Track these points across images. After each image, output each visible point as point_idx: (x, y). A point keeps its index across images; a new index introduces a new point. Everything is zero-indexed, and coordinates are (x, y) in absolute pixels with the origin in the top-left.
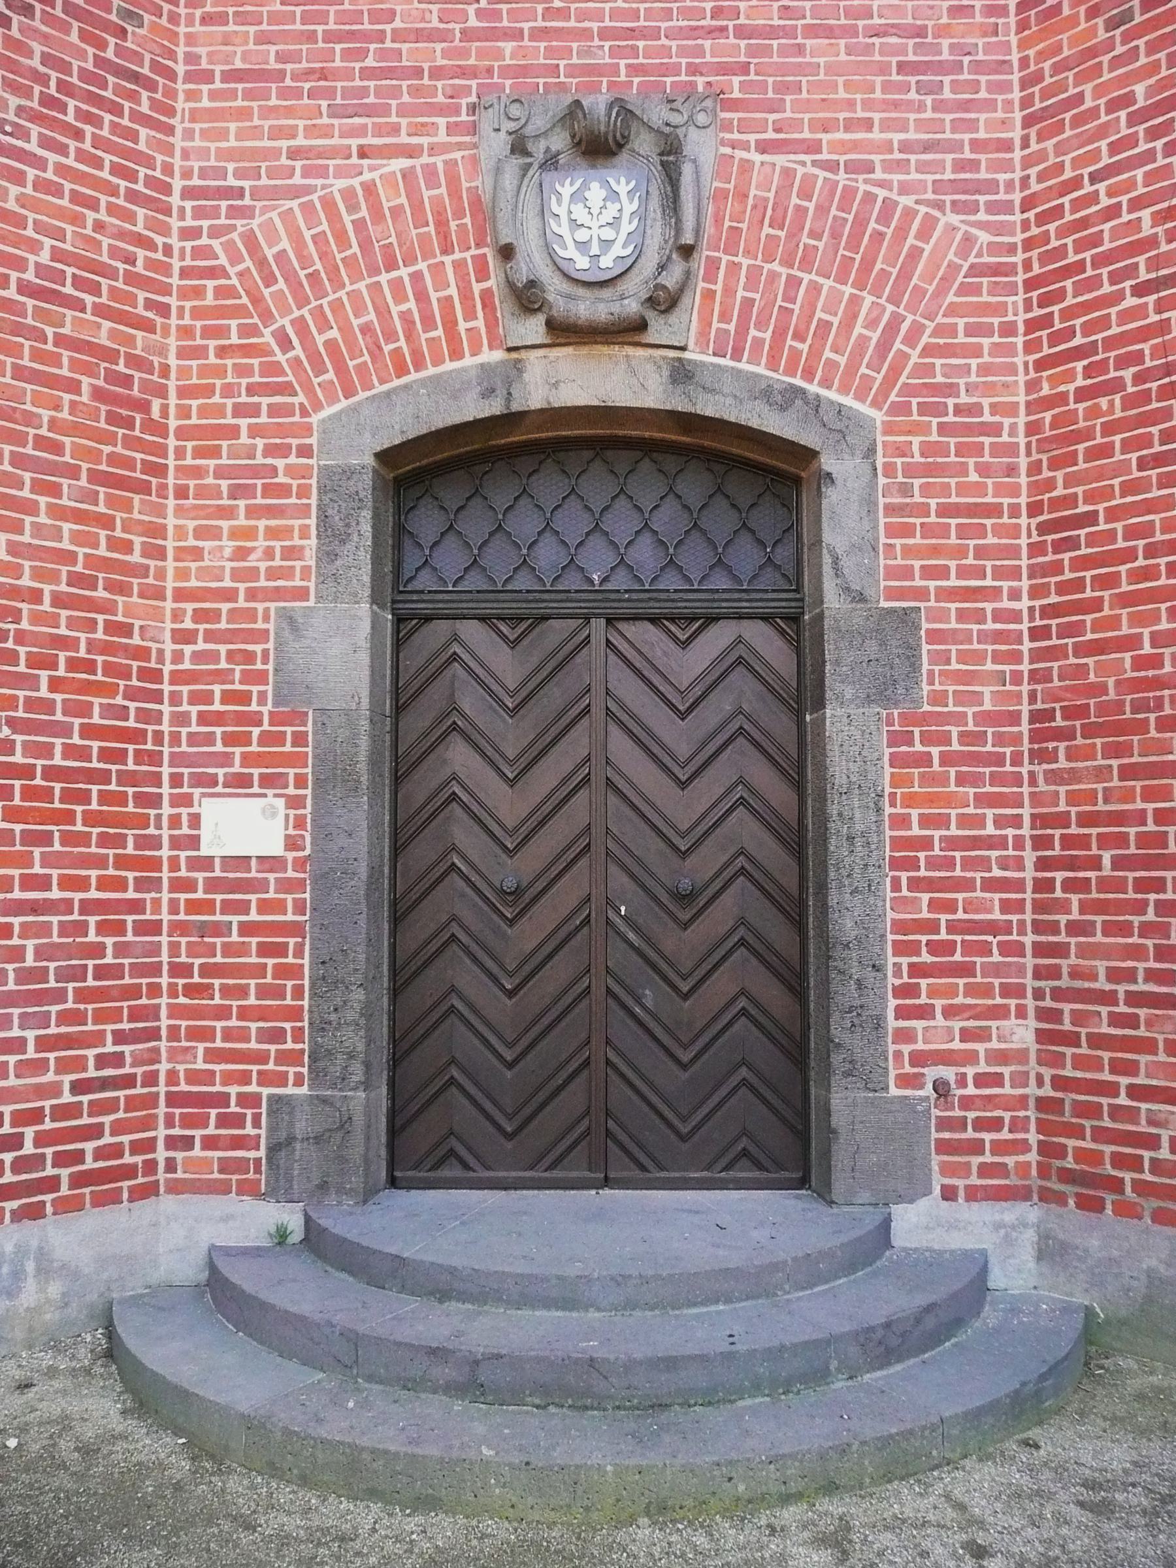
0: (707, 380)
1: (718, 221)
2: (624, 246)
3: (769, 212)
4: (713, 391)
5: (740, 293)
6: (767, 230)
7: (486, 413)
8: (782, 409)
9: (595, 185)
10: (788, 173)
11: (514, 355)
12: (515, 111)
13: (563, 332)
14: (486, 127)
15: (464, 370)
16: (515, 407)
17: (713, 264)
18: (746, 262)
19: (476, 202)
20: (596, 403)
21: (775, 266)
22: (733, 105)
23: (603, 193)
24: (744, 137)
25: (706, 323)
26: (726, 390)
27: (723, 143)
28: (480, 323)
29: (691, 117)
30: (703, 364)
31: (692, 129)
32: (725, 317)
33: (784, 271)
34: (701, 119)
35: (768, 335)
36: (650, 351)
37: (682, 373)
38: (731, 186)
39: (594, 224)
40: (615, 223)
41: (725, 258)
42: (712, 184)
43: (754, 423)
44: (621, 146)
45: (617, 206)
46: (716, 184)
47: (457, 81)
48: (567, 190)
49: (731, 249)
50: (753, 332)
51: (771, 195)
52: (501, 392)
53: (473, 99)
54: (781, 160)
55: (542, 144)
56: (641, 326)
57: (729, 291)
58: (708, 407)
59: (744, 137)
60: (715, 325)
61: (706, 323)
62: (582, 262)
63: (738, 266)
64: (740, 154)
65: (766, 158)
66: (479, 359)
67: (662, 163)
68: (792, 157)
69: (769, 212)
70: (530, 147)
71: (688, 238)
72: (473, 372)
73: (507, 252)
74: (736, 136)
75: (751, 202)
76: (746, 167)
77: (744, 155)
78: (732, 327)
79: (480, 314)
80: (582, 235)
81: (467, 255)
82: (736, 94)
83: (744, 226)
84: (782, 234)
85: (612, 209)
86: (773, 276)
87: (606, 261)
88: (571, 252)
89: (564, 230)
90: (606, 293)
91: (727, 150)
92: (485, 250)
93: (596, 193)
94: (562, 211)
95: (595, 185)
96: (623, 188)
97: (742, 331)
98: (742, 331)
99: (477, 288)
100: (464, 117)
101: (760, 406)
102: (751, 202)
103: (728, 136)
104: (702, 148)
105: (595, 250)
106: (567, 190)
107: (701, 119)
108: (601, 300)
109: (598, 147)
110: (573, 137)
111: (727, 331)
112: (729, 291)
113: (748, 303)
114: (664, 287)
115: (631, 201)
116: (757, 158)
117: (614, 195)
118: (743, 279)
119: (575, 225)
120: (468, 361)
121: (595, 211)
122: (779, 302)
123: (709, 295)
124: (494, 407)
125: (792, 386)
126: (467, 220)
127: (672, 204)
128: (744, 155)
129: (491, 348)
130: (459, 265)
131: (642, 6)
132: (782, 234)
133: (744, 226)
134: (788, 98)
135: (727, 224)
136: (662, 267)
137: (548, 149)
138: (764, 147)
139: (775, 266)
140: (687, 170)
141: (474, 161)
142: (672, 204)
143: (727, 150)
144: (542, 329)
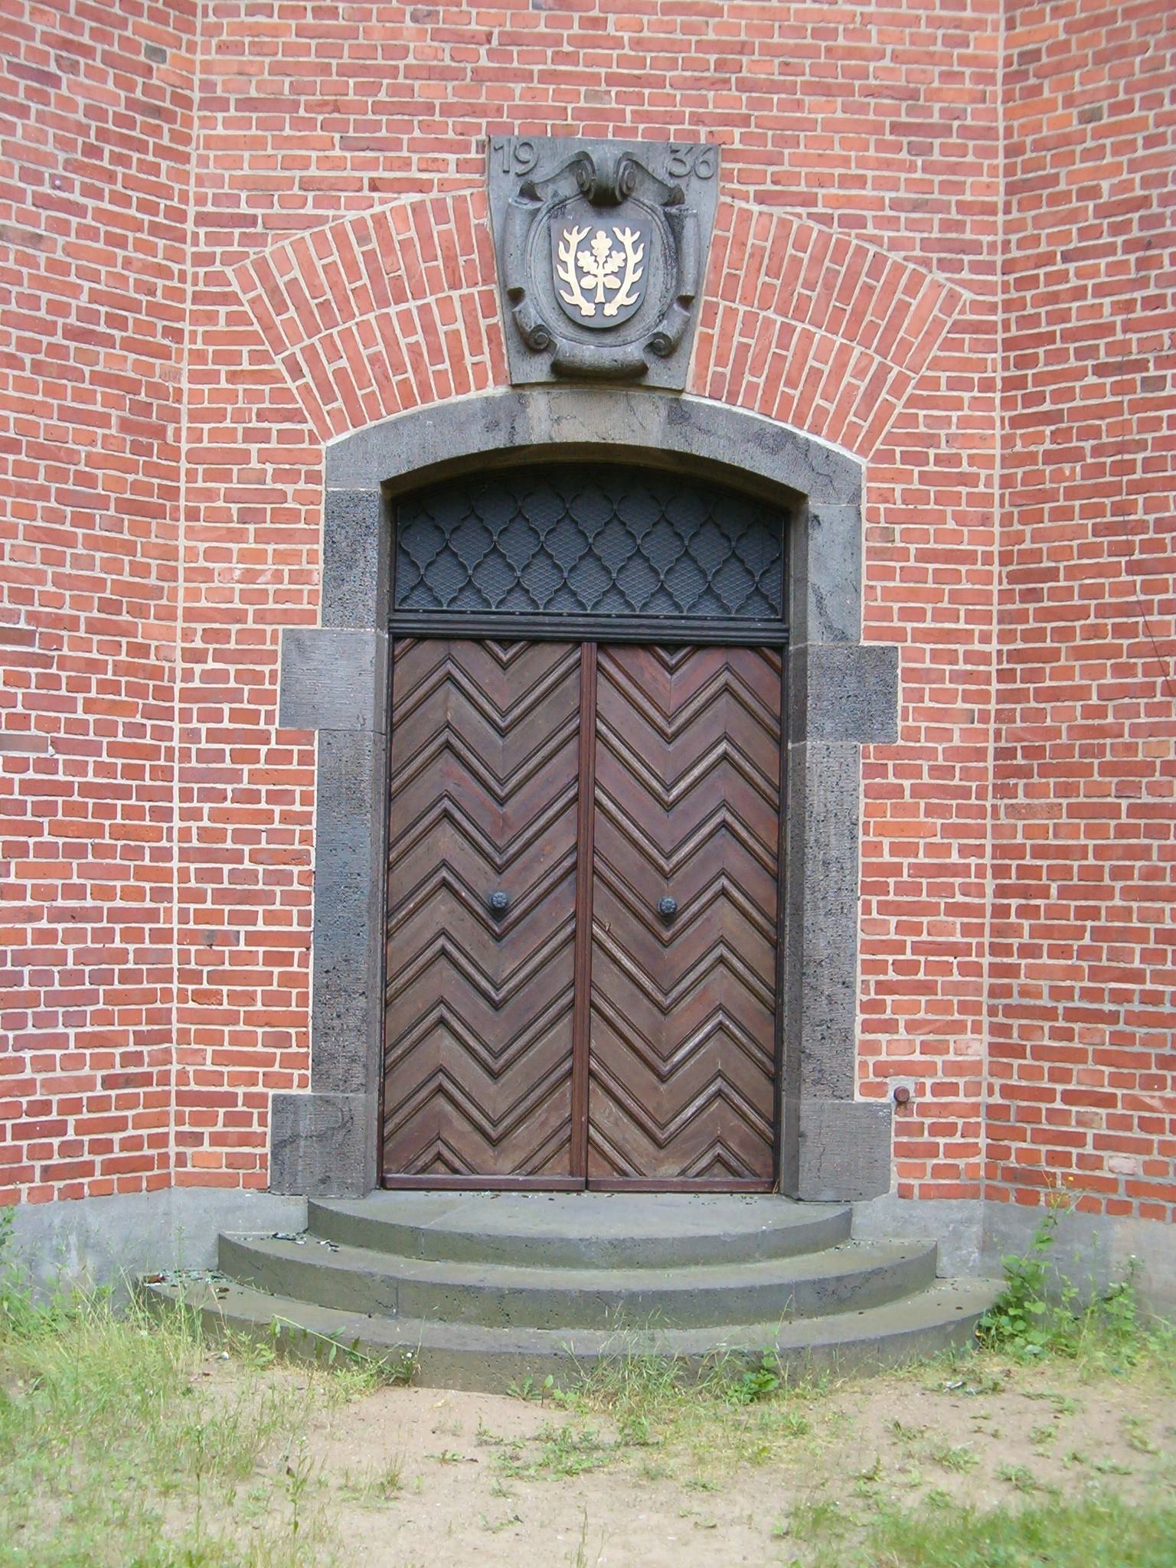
1: (717, 267)
2: (628, 295)
3: (766, 261)
6: (764, 278)
7: (491, 447)
8: (774, 451)
9: (601, 234)
12: (524, 154)
14: (496, 169)
15: (469, 402)
16: (519, 441)
17: (711, 308)
18: (742, 309)
20: (595, 440)
21: (770, 314)
23: (609, 243)
25: (702, 365)
28: (486, 357)
29: (693, 168)
32: (721, 361)
33: (780, 319)
35: (762, 381)
37: (679, 413)
38: (730, 235)
39: (600, 272)
40: (620, 274)
41: (723, 304)
43: (747, 466)
44: (625, 196)
46: (716, 232)
48: (574, 238)
50: (748, 377)
52: (505, 425)
53: (483, 137)
54: (778, 211)
55: (551, 189)
56: (641, 370)
57: (726, 336)
58: (702, 447)
59: (744, 188)
60: (712, 368)
61: (702, 365)
62: (588, 309)
65: (764, 208)
67: (668, 216)
68: (789, 209)
69: (766, 261)
71: (688, 290)
73: (515, 296)
74: (736, 186)
75: (748, 250)
76: (745, 216)
77: (744, 205)
78: (728, 371)
79: (486, 349)
80: (588, 282)
81: (474, 290)
82: (737, 145)
83: (742, 273)
85: (617, 259)
86: (768, 323)
88: (577, 299)
89: (570, 277)
90: (609, 339)
91: (728, 200)
93: (602, 242)
94: (568, 258)
95: (601, 234)
96: (628, 239)
98: (738, 374)
99: (483, 323)
100: (473, 155)
102: (748, 250)
103: (729, 186)
104: (701, 201)
105: (600, 297)
106: (574, 238)
107: (703, 171)
109: (605, 200)
110: (581, 185)
114: (665, 337)
116: (756, 208)
117: (618, 246)
118: (739, 325)
119: (581, 272)
120: (473, 394)
121: (601, 261)
122: (773, 349)
123: (707, 339)
124: (497, 441)
125: (783, 430)
126: (475, 256)
127: (675, 254)
128: (744, 205)
129: (496, 382)
133: (742, 273)
134: (786, 152)
135: (725, 271)
136: (663, 315)
137: (555, 194)
138: (762, 198)
139: (770, 314)
140: (689, 225)
142: (675, 254)
143: (728, 200)
144: (546, 368)
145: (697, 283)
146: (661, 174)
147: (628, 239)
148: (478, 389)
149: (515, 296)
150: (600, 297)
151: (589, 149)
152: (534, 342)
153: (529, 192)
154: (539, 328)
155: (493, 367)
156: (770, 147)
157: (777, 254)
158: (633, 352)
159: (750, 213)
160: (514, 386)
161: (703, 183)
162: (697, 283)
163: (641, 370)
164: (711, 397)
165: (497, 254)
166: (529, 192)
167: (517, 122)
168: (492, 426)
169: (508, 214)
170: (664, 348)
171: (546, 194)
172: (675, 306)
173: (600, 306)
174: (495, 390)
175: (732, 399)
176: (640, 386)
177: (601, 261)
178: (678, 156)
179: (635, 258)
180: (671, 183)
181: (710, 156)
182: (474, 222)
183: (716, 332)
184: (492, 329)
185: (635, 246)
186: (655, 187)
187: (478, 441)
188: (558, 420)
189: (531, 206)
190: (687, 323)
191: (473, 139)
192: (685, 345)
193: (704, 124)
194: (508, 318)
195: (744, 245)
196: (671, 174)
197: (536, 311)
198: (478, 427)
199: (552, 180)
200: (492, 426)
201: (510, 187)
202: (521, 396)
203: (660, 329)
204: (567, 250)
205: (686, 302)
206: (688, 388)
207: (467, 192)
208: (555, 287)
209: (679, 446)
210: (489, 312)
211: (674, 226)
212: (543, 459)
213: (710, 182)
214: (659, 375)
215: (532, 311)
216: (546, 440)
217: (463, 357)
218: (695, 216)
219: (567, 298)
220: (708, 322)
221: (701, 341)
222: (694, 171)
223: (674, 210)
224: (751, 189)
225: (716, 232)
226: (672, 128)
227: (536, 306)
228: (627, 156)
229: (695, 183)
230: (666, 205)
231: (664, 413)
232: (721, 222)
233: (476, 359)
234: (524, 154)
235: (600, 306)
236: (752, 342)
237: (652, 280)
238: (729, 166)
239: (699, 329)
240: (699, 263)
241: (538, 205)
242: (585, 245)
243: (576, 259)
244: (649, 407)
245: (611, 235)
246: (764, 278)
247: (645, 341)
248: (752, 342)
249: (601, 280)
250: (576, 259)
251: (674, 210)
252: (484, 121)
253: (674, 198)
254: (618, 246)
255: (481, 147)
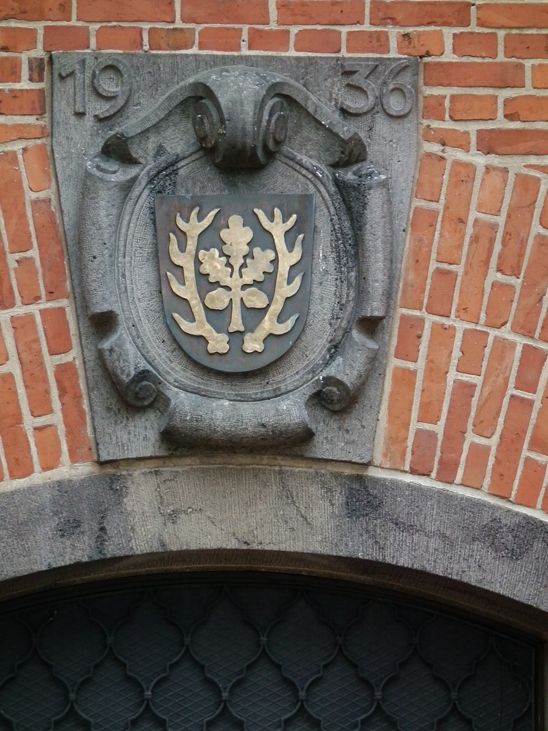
0: (402, 512)
1: (419, 261)
2: (281, 319)
3: (498, 247)
4: (410, 528)
5: (452, 375)
6: (494, 276)
7: (67, 560)
8: (515, 555)
9: (235, 220)
10: (527, 185)
11: (110, 470)
12: (109, 86)
13: (182, 443)
14: (63, 108)
15: (32, 490)
16: (112, 549)
17: (412, 327)
18: (461, 327)
19: (49, 227)
20: (232, 544)
21: (506, 333)
22: (445, 74)
23: (248, 234)
24: (460, 127)
25: (400, 421)
26: (430, 527)
27: (429, 135)
28: (56, 418)
29: (379, 99)
30: (395, 485)
31: (380, 119)
32: (428, 413)
33: (520, 341)
34: (395, 104)
35: (493, 442)
36: (316, 466)
37: (362, 495)
38: (440, 206)
39: (235, 282)
40: (267, 283)
41: (430, 320)
42: (408, 203)
43: (472, 578)
44: (270, 155)
45: (271, 255)
46: (418, 203)
47: (13, 24)
48: (193, 227)
49: (440, 307)
50: (471, 438)
51: (501, 220)
52: (89, 526)
53: (39, 52)
54: (516, 164)
55: (152, 143)
56: (306, 436)
57: (435, 372)
58: (403, 552)
59: (460, 127)
60: (414, 425)
61: (400, 421)
62: (218, 343)
63: (450, 331)
64: (454, 154)
65: (494, 160)
66: (54, 475)
67: (337, 182)
68: (533, 160)
69: (498, 247)
70: (135, 151)
71: (375, 308)
72: (47, 495)
73: (103, 324)
74: (448, 125)
75: (469, 230)
76: (464, 174)
77: (461, 156)
78: (439, 428)
79: (56, 405)
80: (218, 299)
81: (34, 309)
82: (449, 57)
83: (459, 269)
84: (517, 282)
85: (263, 259)
86: (503, 348)
87: (253, 344)
88: (199, 326)
89: (187, 291)
90: (252, 389)
91: (435, 148)
92: (64, 303)
93: (237, 235)
94: (184, 260)
95: (235, 220)
96: (278, 229)
97: (454, 434)
98: (454, 434)
99: (51, 363)
100: (24, 84)
101: (481, 551)
102: (469, 230)
103: (435, 124)
104: (396, 155)
105: (237, 323)
106: (193, 227)
107: (395, 104)
108: (245, 399)
109: (239, 161)
110: (202, 139)
111: (432, 435)
112: (435, 372)
113: (465, 390)
114: (339, 383)
115: (291, 247)
116: (480, 160)
117: (262, 238)
118: (456, 353)
119: (205, 283)
120: (38, 477)
121: (237, 263)
122: (511, 391)
123: (406, 378)
124: (78, 550)
125: (527, 518)
126: (34, 253)
127: (352, 247)
128: (461, 156)
129: (74, 457)
130: (21, 325)
131: (537, 398)
132: (517, 282)
133: (459, 269)
134: (528, 64)
135: (433, 266)
136: (335, 348)
137: (160, 151)
138: (489, 143)
139: (506, 333)
140: (375, 200)
141: (48, 157)
142: (352, 247)
143: (435, 148)
144: (153, 435)
145: (389, 295)
146: (329, 115)
147: (278, 229)
148: (46, 468)
149: (103, 324)
150: (237, 323)
151: (212, 78)
152: (134, 396)
153: (117, 151)
154: (143, 375)
155: (70, 433)
156: (501, 57)
157: (514, 236)
158: (290, 410)
159: (470, 167)
160: (102, 464)
161: (396, 125)
162: (389, 295)
163: (306, 436)
164: (413, 471)
165: (71, 254)
166: (117, 151)
167: (94, 27)
168: (69, 528)
169: (87, 187)
170: (336, 401)
171: (145, 151)
172: (356, 334)
173: (237, 337)
174: (73, 470)
175: (447, 473)
176: (302, 457)
177: (237, 263)
178: (356, 80)
179: (288, 259)
180: (345, 129)
181: (406, 79)
182: (30, 196)
183: (420, 366)
184: (64, 371)
185: (290, 237)
186: (317, 136)
187: (46, 552)
188: (173, 517)
189: (120, 174)
190: (375, 362)
191: (24, 57)
192: (371, 392)
193: (395, 22)
194: (90, 356)
195: (462, 221)
196: (345, 112)
197: (139, 345)
198: (46, 530)
199: (156, 128)
200: (69, 528)
201: (80, 141)
202: (113, 479)
203: (331, 371)
204: (182, 248)
205: (371, 326)
206: (377, 462)
207: (17, 147)
208: (168, 307)
209: (363, 550)
210: (59, 344)
211: (351, 201)
212: (144, 570)
213: (407, 124)
214: (330, 442)
215: (130, 348)
216: (156, 548)
217: (18, 418)
218: (384, 184)
219: (186, 326)
220: (407, 352)
221: (396, 380)
222: (380, 107)
223: (349, 176)
224: (473, 128)
225: (418, 203)
226: (344, 30)
227: (136, 337)
228: (276, 91)
229: (382, 125)
230: (335, 166)
231: (339, 499)
232: (423, 188)
233: (41, 421)
234: (109, 86)
235: (237, 337)
236: (477, 380)
237: (317, 291)
238: (437, 91)
239: (394, 363)
240: (391, 260)
241: (133, 171)
242: (211, 238)
243: (198, 262)
244: (315, 490)
245: (252, 221)
246: (494, 276)
247: (307, 390)
248: (477, 380)
249: (237, 294)
250: (198, 262)
251: (349, 176)
252: (39, 26)
253: (350, 154)
254: (262, 238)
255: (38, 69)
